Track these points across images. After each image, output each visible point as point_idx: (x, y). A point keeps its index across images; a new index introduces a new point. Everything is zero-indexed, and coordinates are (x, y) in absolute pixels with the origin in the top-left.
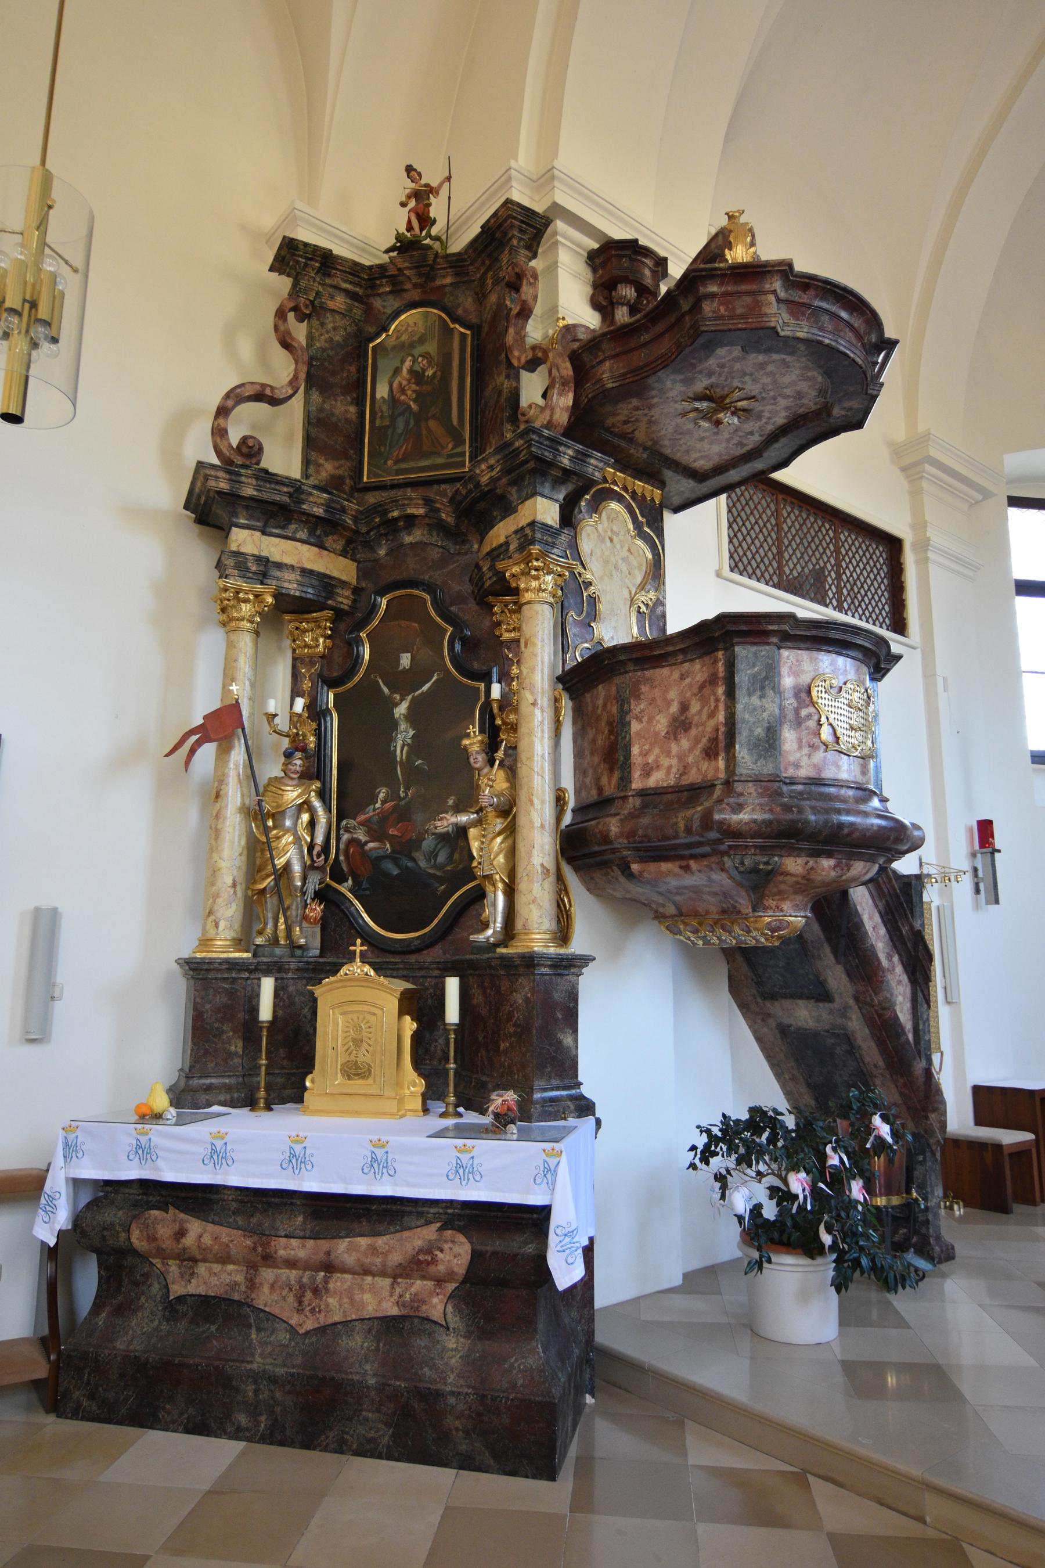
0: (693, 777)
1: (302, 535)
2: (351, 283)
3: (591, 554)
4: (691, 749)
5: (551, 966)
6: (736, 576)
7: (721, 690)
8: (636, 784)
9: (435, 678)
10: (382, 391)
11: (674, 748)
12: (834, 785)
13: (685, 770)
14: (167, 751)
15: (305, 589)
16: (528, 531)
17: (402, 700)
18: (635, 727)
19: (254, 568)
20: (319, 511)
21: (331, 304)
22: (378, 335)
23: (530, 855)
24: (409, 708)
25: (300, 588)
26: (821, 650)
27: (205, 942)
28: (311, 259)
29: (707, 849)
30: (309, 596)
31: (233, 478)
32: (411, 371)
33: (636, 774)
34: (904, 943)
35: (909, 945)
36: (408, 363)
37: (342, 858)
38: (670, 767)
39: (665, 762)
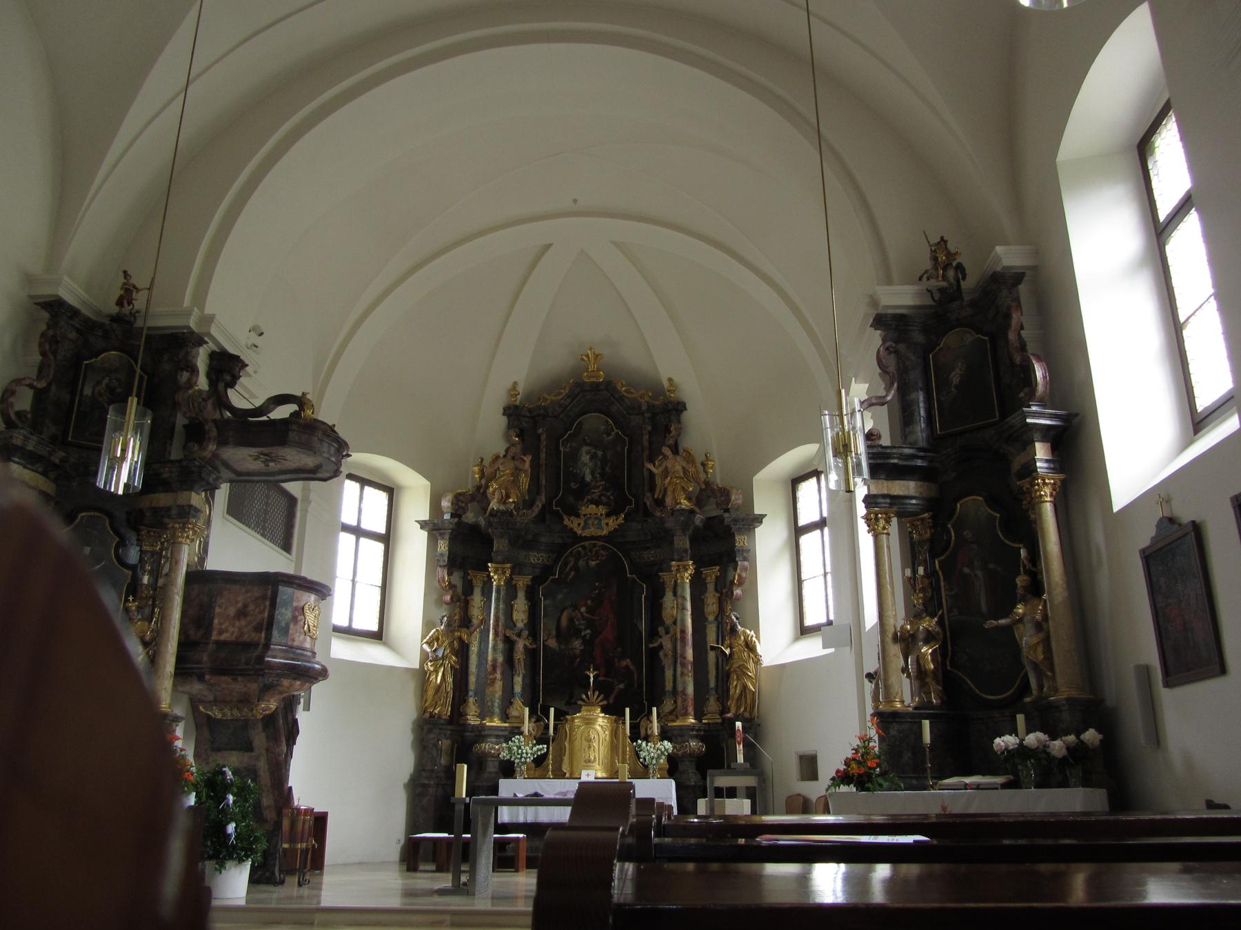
0: (246, 638)
4: (246, 626)
7: (268, 603)
8: (214, 637)
9: (103, 563)
10: (88, 391)
11: (237, 624)
13: (242, 634)
16: (186, 508)
18: (218, 610)
20: (57, 461)
22: (90, 358)
23: (165, 666)
29: (253, 672)
32: (107, 385)
33: (215, 633)
34: (288, 725)
35: (290, 726)
36: (106, 381)
38: (233, 632)
39: (231, 629)
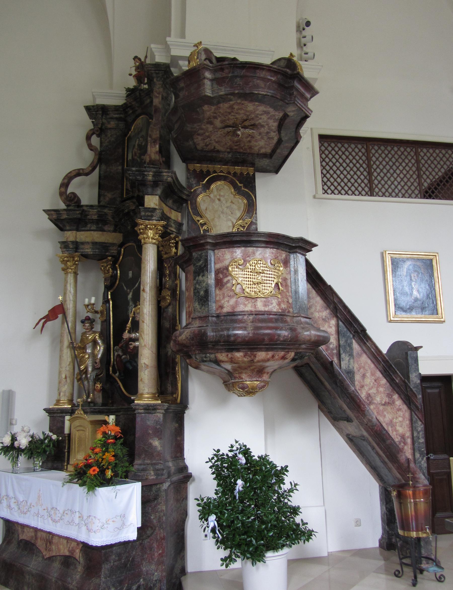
1: (94, 227)
2: (117, 114)
3: (206, 209)
5: (144, 409)
6: (326, 196)
10: (130, 157)
12: (240, 315)
14: (34, 326)
15: (94, 251)
17: (130, 292)
19: (71, 247)
20: (95, 217)
21: (109, 126)
24: (133, 295)
25: (93, 250)
26: (235, 247)
27: (58, 402)
28: (97, 111)
30: (97, 253)
31: (58, 213)
32: (138, 145)
34: (399, 387)
37: (115, 363)
